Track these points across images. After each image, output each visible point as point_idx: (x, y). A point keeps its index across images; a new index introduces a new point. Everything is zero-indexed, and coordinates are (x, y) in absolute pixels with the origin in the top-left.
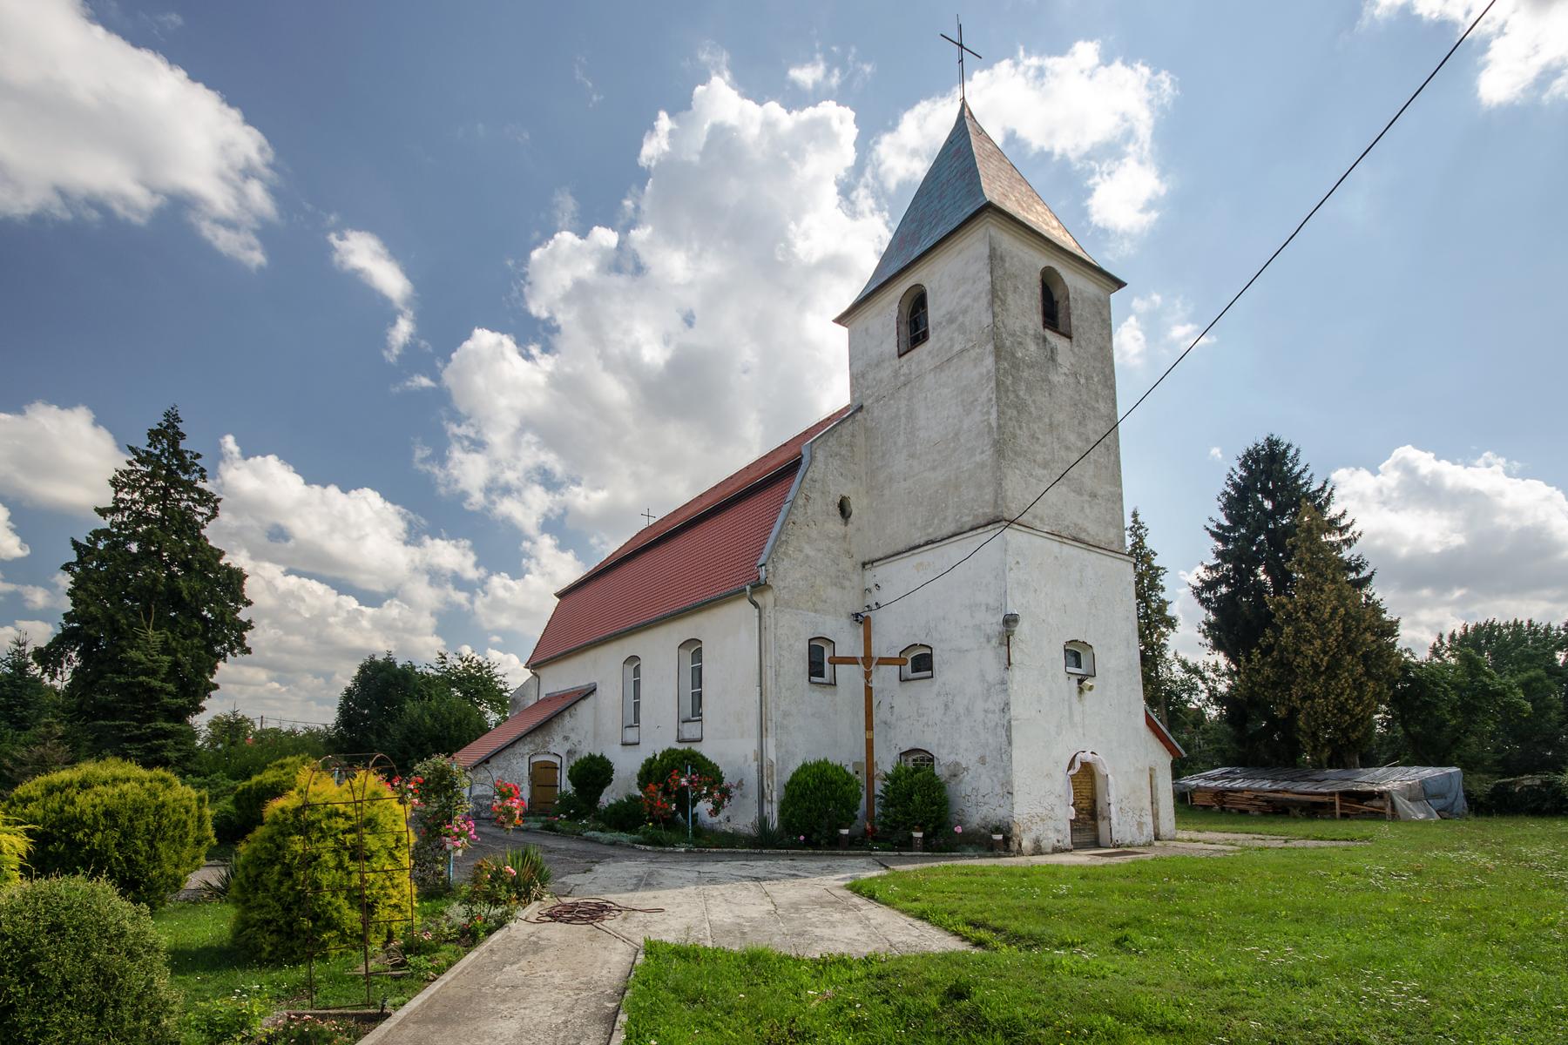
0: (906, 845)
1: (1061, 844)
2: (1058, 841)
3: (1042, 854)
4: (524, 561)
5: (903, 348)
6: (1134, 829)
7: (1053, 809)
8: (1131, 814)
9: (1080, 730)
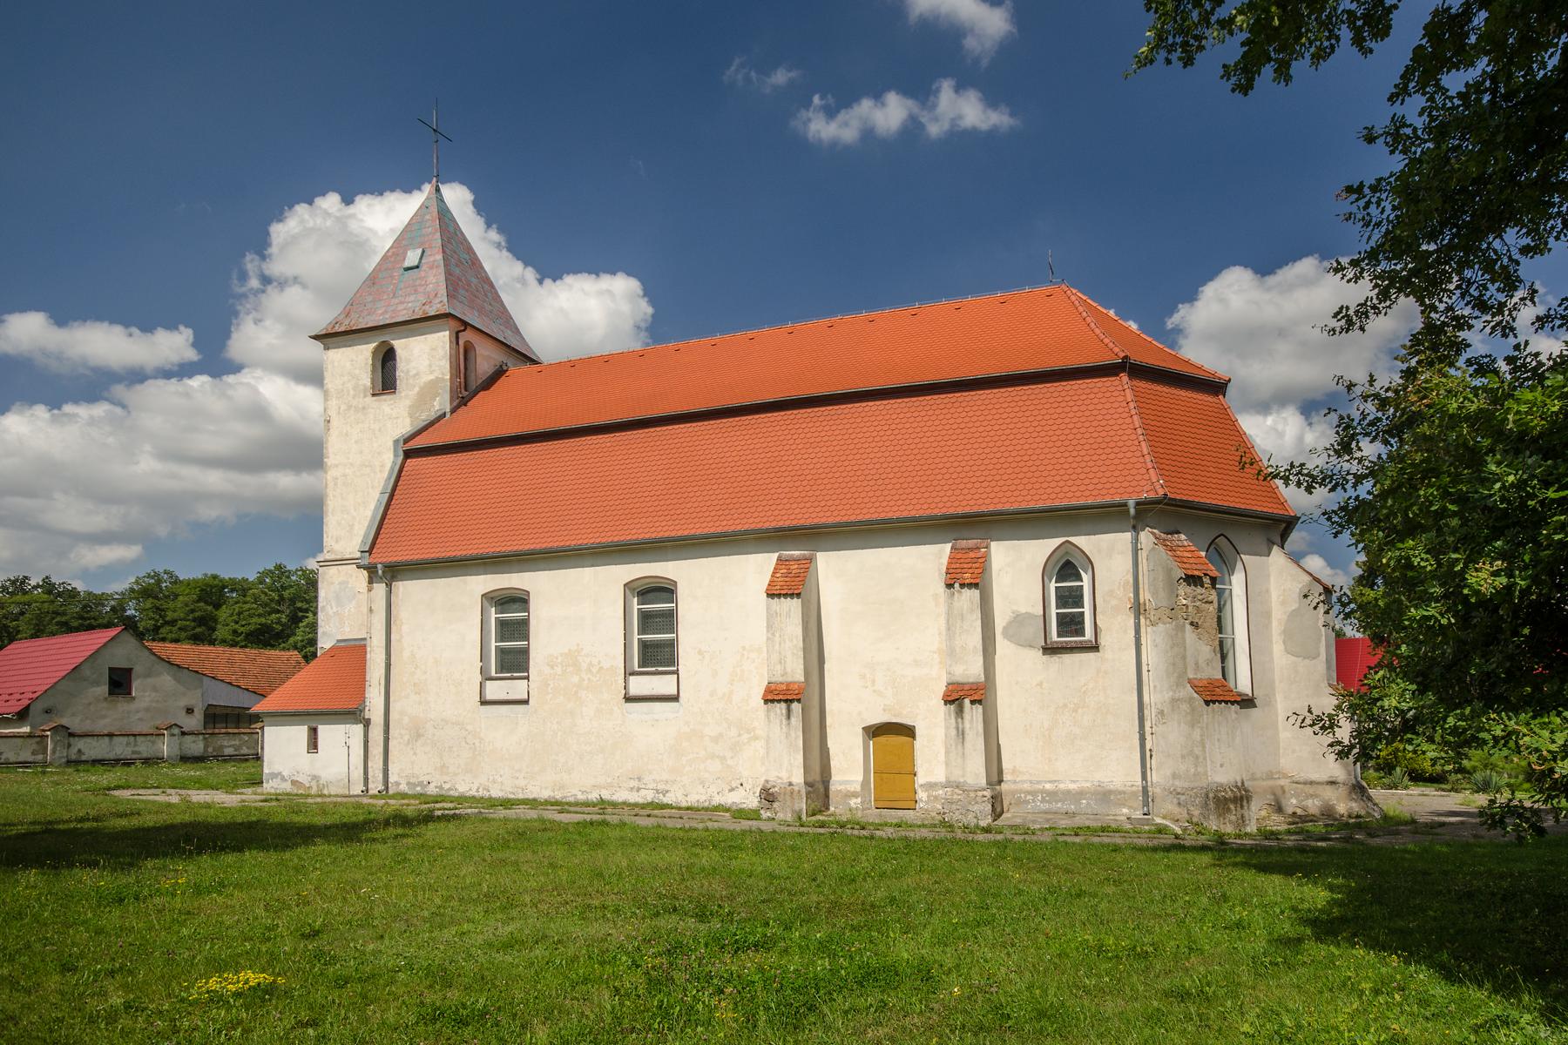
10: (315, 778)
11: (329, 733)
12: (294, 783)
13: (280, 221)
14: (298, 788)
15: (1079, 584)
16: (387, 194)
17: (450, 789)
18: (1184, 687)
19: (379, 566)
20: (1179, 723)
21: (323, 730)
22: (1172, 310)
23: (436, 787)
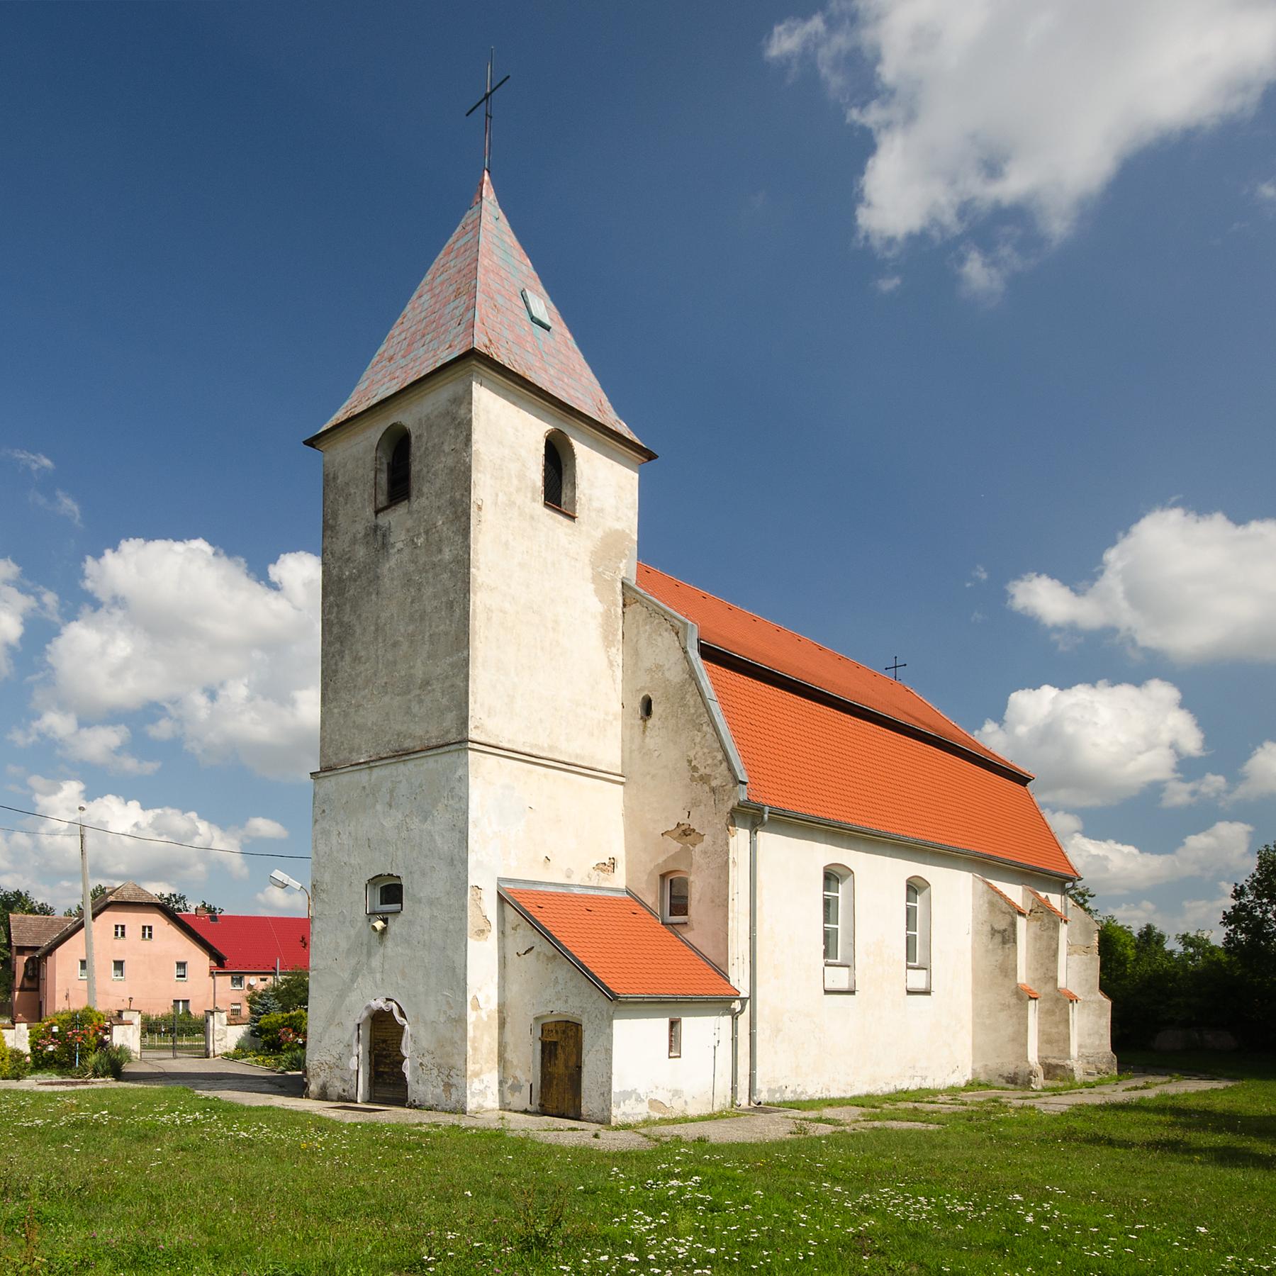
0: (1205, 1128)
1: (346, 1094)
2: (344, 1091)
3: (327, 1100)
4: (1221, 804)
5: (383, 499)
6: (439, 1091)
7: (340, 1058)
8: (435, 1072)
9: (378, 976)
10: (677, 1093)
11: (697, 1028)
12: (654, 1104)
13: (878, 59)
14: (659, 1111)
15: (835, 926)
16: (156, 541)
17: (802, 1093)
18: (1095, 994)
19: (767, 809)
20: (1089, 1015)
21: (690, 1025)
22: (1201, 758)
23: (792, 1092)
